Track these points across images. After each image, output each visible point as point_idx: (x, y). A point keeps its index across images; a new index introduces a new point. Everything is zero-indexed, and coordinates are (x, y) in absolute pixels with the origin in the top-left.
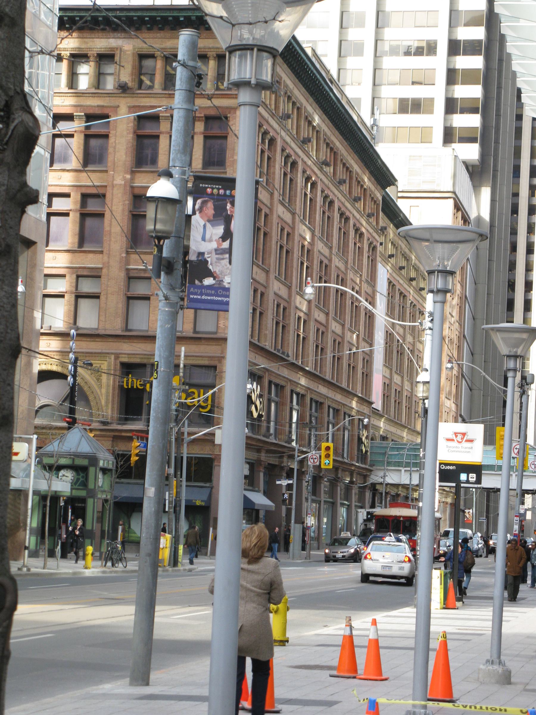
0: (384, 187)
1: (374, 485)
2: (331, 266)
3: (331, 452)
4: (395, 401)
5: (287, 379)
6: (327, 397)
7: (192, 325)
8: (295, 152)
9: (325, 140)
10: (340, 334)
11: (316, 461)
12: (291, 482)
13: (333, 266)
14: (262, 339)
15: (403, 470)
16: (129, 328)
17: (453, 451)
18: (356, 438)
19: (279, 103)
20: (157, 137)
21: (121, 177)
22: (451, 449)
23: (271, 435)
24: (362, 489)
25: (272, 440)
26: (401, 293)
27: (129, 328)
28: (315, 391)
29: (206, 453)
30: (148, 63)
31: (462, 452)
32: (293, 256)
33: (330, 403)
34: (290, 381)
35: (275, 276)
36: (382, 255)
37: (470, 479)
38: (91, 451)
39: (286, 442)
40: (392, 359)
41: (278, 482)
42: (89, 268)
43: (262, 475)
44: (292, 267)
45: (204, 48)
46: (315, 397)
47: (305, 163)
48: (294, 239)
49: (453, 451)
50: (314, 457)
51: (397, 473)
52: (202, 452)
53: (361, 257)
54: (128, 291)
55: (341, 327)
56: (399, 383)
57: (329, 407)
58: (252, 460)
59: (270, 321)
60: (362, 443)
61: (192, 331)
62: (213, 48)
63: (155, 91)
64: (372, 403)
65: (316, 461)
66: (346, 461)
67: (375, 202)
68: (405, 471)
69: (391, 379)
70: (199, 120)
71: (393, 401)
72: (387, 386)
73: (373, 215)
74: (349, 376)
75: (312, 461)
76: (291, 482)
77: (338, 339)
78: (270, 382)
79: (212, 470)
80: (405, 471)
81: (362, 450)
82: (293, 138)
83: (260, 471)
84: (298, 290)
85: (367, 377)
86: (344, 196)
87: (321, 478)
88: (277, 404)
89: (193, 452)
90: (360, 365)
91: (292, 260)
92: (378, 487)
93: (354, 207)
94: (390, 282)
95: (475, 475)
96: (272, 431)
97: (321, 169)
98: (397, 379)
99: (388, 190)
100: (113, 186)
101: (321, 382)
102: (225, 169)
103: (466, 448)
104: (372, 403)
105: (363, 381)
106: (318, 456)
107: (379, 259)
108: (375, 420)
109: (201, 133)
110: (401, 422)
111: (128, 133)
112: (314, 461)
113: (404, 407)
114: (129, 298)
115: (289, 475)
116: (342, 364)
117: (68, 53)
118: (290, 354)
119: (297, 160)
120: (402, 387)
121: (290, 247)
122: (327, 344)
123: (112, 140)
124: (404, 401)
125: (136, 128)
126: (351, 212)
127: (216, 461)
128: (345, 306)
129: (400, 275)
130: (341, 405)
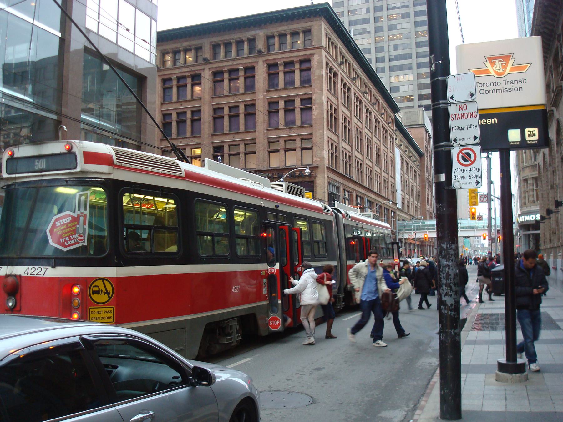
0: (395, 113)
2: (372, 141)
5: (353, 189)
6: (375, 200)
7: (300, 162)
8: (349, 83)
9: (365, 83)
10: (380, 172)
13: (373, 141)
14: (338, 168)
16: (271, 166)
17: (489, 92)
19: (338, 56)
20: (278, 73)
21: (262, 94)
22: (485, 88)
26: (406, 162)
27: (271, 166)
30: (271, 41)
31: (506, 90)
32: (352, 132)
34: (355, 190)
35: (343, 140)
36: (397, 144)
37: (527, 138)
42: (250, 140)
44: (352, 137)
45: (297, 28)
46: (386, 207)
47: (355, 90)
48: (352, 124)
49: (489, 92)
53: (387, 141)
54: (269, 148)
55: (380, 170)
56: (408, 198)
57: (384, 208)
59: (341, 162)
61: (300, 165)
62: (301, 28)
63: (275, 52)
64: (396, 204)
67: (391, 118)
69: (405, 196)
70: (297, 63)
71: (406, 205)
72: (403, 199)
73: (391, 123)
77: (379, 175)
80: (413, 232)
82: (347, 76)
84: (356, 148)
85: (394, 192)
86: (377, 111)
90: (390, 187)
91: (352, 134)
93: (382, 118)
94: (401, 157)
95: (536, 129)
97: (364, 96)
98: (407, 196)
99: (396, 115)
100: (259, 99)
102: (311, 84)
103: (512, 82)
104: (396, 204)
107: (395, 146)
109: (298, 69)
111: (263, 73)
113: (411, 208)
114: (270, 152)
117: (234, 40)
118: (354, 177)
119: (351, 87)
120: (410, 200)
121: (350, 128)
122: (373, 176)
123: (256, 78)
124: (411, 206)
125: (267, 70)
126: (380, 120)
128: (381, 161)
129: (405, 154)
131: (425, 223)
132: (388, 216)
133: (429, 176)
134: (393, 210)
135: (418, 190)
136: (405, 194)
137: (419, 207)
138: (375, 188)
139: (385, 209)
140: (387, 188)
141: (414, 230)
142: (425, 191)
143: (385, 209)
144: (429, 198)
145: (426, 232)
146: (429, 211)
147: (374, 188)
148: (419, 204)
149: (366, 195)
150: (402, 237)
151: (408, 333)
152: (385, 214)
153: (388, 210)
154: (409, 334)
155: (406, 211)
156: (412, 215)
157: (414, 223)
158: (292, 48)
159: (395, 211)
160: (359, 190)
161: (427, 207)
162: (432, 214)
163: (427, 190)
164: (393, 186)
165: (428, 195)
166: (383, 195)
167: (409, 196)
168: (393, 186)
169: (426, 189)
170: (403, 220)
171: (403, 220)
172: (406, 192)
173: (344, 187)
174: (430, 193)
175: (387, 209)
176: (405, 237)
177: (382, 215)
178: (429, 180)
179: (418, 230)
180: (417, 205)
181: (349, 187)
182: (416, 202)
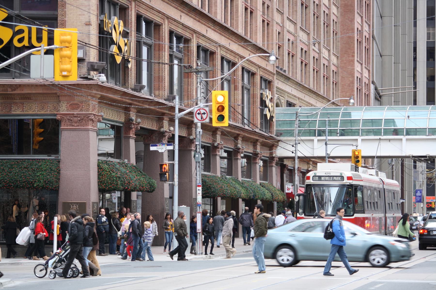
1: (282, 159)
3: (226, 113)
4: (302, 62)
11: (204, 116)
12: (171, 148)
15: (316, 139)
18: (259, 100)
23: (143, 87)
24: (267, 163)
25: (144, 94)
28: (203, 36)
29: (49, 112)
33: (224, 54)
34: (168, 18)
38: (263, 239)
39: (165, 100)
40: (296, 11)
41: (152, 148)
43: (132, 143)
46: (204, 43)
50: (202, 111)
51: (309, 144)
52: (42, 112)
57: (222, 58)
58: (116, 122)
60: (266, 106)
65: (204, 116)
66: (246, 127)
68: (318, 140)
74: (246, 22)
75: (199, 117)
76: (171, 148)
78: (139, 17)
79: (58, 137)
81: (266, 115)
83: (129, 137)
87: (216, 148)
88: (150, 47)
89: (31, 112)
92: (286, 162)
96: (145, 82)
101: (210, 24)
105: (263, 31)
106: (207, 109)
108: (280, 82)
110: (309, 86)
112: (202, 118)
115: (171, 141)
116: (237, 6)
127: (63, 124)
130: (237, 57)
131: (349, 114)
132: (251, 92)
133: (365, 25)
134: (267, 77)
135: (333, 17)
136: (296, 29)
137: (333, 68)
138: (219, 11)
139: (225, 63)
140: (251, 12)
141: (321, 133)
142: (352, 20)
143: (225, 63)
144: (360, 43)
145: (357, 140)
146: (360, 80)
147: (216, 13)
148: (334, 60)
149: (195, 31)
150: (293, 155)
151: (332, 274)
152: (243, 87)
153: (252, 75)
154: (333, 275)
155: (299, 79)
156: (315, 90)
157: (103, 47)
158: (392, 160)
159: (270, 78)
160: (177, 17)
161: (357, 67)
162: (369, 90)
163: (358, 19)
164: (268, 7)
165: (360, 32)
166: (240, 31)
167: (308, 34)
168: (268, 7)
169: (356, 15)
170: (290, 104)
171: (290, 104)
172: (299, 25)
173: (200, 41)
174: (366, 27)
175: (248, 72)
176: (300, 155)
177: (236, 88)
178: (365, 34)
179: (331, 133)
180: (329, 61)
181: (153, 8)
182: (325, 53)
